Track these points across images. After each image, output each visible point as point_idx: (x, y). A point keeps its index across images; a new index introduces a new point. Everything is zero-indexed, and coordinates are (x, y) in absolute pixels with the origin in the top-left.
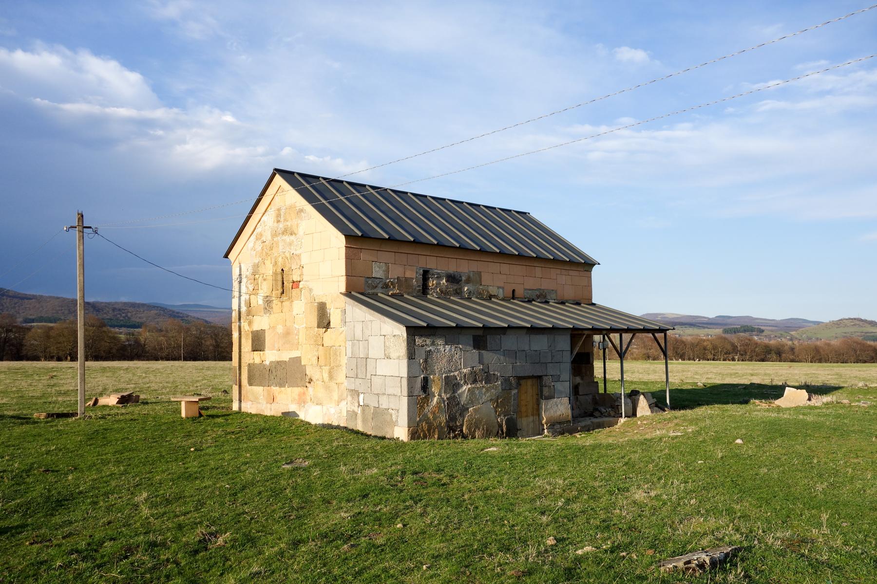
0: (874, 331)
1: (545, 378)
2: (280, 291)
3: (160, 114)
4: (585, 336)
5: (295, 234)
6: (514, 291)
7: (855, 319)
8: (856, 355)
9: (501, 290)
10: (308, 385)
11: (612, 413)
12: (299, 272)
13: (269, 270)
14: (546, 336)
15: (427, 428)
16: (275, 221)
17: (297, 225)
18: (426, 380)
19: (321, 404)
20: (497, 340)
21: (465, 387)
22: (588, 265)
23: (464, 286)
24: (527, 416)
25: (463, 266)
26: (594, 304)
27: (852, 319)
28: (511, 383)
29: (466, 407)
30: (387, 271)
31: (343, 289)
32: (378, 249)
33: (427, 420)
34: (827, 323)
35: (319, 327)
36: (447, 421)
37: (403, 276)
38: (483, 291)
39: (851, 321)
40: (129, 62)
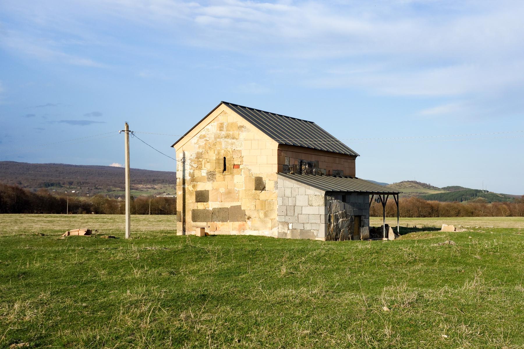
0: (425, 192)
2: (222, 168)
5: (237, 139)
7: (412, 182)
8: (419, 211)
10: (246, 220)
11: (378, 236)
12: (239, 160)
13: (212, 156)
16: (218, 129)
17: (239, 134)
19: (257, 230)
22: (353, 156)
25: (313, 158)
26: (357, 178)
27: (410, 182)
31: (277, 171)
34: (391, 185)
35: (256, 189)
39: (409, 183)
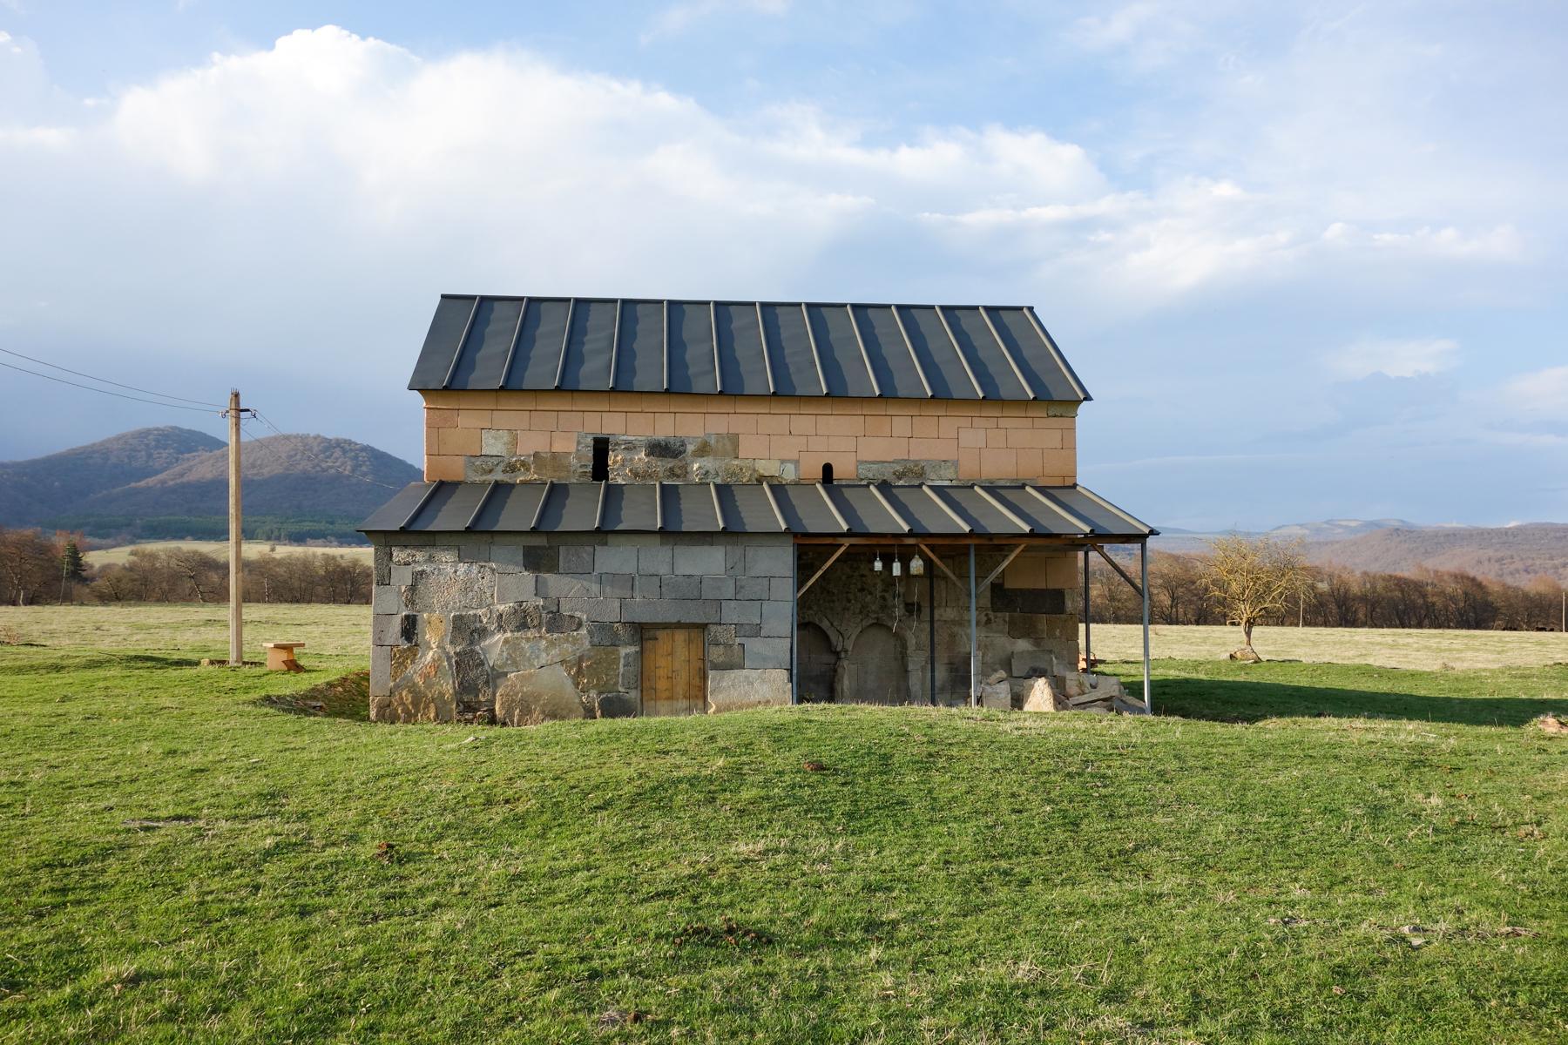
1: (713, 628)
3: (1107, 205)
4: (842, 549)
9: (790, 467)
15: (410, 700)
21: (497, 637)
23: (693, 462)
24: (671, 698)
28: (616, 634)
29: (501, 671)
30: (514, 442)
32: (494, 408)
33: (413, 689)
36: (456, 693)
37: (548, 450)
38: (741, 469)
40: (1059, 132)
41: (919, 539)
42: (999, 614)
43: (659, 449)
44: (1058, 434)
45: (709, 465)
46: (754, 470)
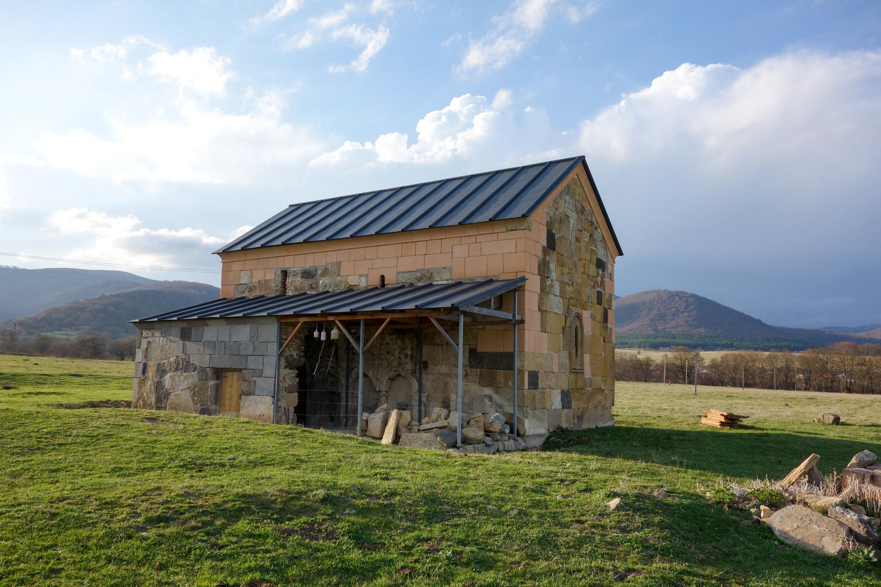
1: (244, 371)
4: (299, 324)
6: (383, 278)
9: (364, 279)
14: (249, 326)
18: (145, 365)
20: (200, 332)
23: (320, 280)
30: (252, 276)
41: (335, 317)
42: (473, 370)
43: (308, 274)
44: (513, 242)
45: (327, 281)
46: (347, 282)
